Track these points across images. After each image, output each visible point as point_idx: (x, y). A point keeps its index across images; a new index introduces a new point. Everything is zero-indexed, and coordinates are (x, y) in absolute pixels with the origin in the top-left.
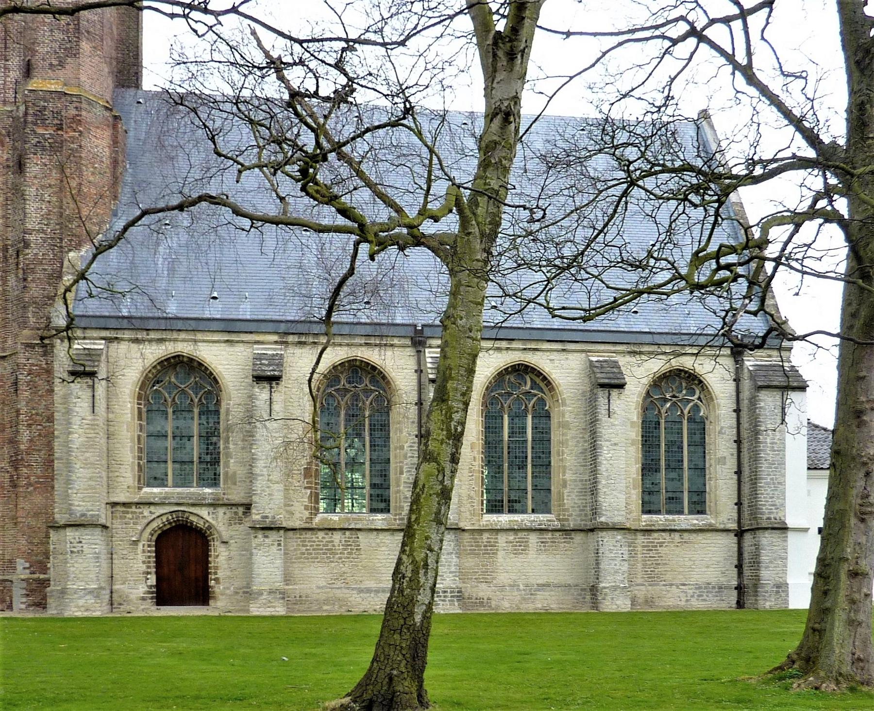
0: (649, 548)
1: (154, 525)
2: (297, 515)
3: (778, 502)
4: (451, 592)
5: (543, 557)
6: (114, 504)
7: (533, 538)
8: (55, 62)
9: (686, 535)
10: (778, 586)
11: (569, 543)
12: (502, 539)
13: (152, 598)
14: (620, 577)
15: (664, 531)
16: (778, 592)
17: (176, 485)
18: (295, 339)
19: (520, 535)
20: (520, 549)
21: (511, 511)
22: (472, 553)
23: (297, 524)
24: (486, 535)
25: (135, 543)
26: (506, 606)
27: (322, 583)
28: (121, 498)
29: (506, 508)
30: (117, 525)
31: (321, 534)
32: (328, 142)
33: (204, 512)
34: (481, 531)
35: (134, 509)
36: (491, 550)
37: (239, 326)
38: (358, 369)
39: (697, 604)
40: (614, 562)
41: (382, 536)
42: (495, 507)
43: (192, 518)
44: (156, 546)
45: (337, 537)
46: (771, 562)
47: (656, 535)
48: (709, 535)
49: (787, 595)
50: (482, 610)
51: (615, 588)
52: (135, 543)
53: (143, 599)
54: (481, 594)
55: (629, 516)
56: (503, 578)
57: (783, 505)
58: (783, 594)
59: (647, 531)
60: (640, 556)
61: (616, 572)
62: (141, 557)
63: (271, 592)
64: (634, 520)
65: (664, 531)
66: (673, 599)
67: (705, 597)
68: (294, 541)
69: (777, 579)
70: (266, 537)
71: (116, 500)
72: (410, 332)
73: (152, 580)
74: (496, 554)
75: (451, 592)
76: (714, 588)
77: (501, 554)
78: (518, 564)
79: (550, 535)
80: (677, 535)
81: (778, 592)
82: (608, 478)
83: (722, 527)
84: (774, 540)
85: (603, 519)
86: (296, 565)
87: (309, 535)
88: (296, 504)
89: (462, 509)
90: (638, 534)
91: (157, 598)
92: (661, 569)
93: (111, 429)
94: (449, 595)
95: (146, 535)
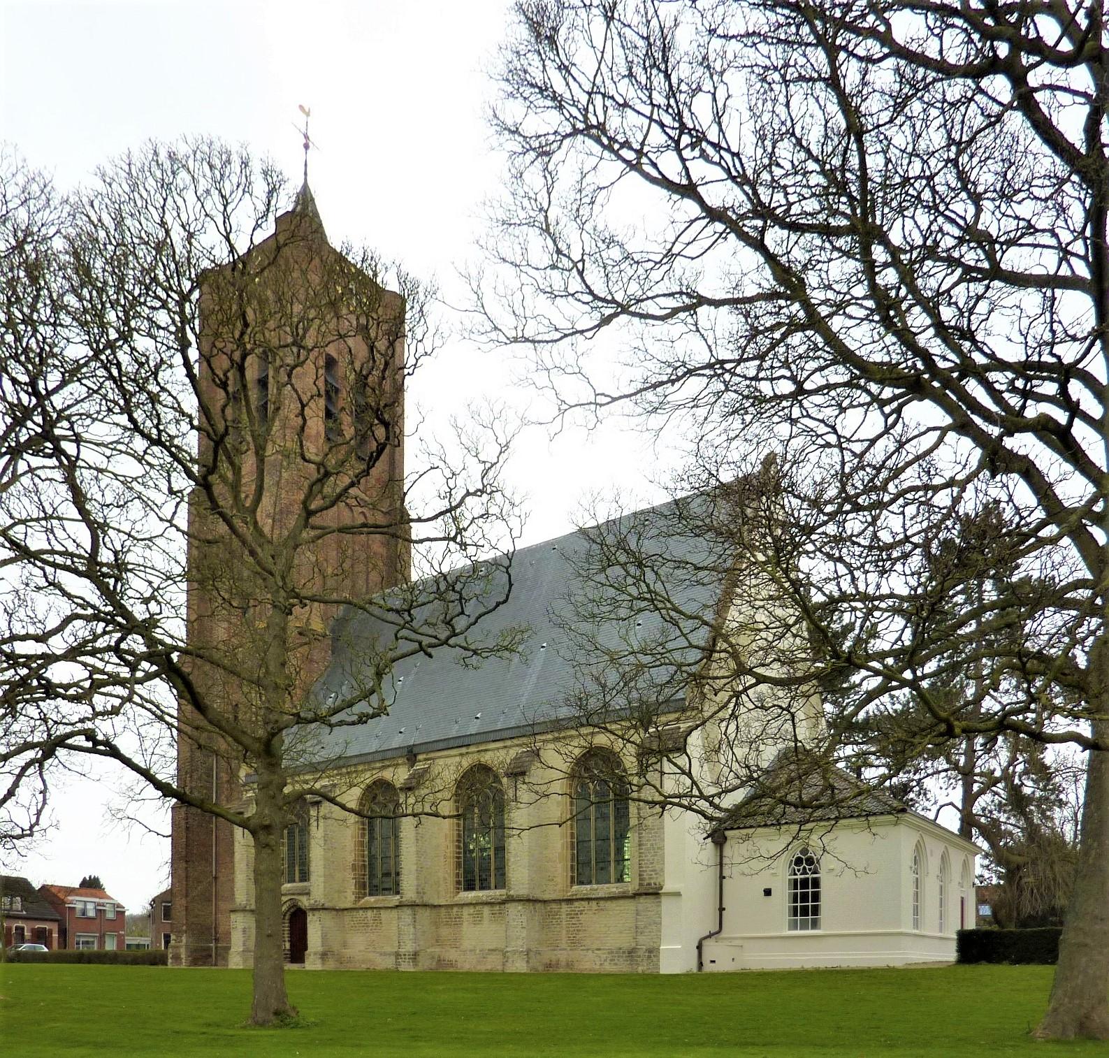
0: (571, 916)
3: (657, 867)
7: (486, 910)
9: (602, 903)
10: (650, 951)
12: (466, 912)
14: (520, 942)
15: (582, 899)
16: (649, 957)
18: (378, 765)
19: (478, 908)
20: (477, 919)
21: (482, 888)
24: (455, 909)
27: (362, 948)
32: (995, 424)
36: (457, 922)
37: (431, 747)
38: (593, 753)
39: (609, 968)
42: (470, 887)
45: (369, 913)
47: (576, 904)
48: (621, 902)
50: (451, 970)
51: (515, 952)
56: (466, 944)
57: (662, 870)
59: (569, 901)
65: (582, 899)
66: (590, 962)
72: (405, 752)
77: (465, 924)
80: (594, 903)
81: (649, 957)
82: (516, 855)
92: (581, 935)
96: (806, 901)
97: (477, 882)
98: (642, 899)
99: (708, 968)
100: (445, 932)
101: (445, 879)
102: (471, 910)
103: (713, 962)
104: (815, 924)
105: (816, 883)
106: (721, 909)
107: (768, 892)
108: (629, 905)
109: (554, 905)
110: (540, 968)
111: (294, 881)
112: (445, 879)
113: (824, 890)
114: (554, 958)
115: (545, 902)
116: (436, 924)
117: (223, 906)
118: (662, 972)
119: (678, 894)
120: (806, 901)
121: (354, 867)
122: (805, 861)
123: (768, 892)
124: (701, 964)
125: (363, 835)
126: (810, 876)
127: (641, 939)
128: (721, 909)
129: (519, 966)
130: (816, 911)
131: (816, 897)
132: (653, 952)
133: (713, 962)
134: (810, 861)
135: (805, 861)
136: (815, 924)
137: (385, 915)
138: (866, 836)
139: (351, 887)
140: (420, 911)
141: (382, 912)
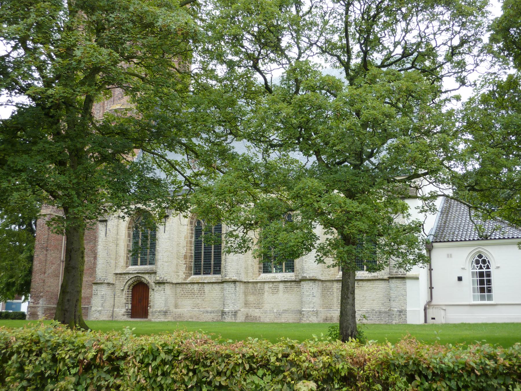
1: (129, 282)
2: (181, 277)
4: (232, 313)
5: (286, 295)
6: (116, 274)
7: (281, 285)
8: (120, 97)
10: (400, 312)
11: (299, 288)
12: (266, 286)
13: (128, 315)
17: (141, 264)
19: (275, 284)
20: (275, 291)
22: (253, 294)
23: (180, 281)
24: (259, 285)
25: (123, 290)
26: (267, 320)
27: (189, 309)
28: (119, 271)
29: (202, 272)
30: (117, 282)
31: (189, 285)
33: (146, 277)
34: (257, 283)
35: (123, 276)
36: (261, 292)
40: (308, 298)
41: (214, 285)
42: (197, 273)
43: (142, 279)
44: (132, 292)
45: (196, 286)
46: (396, 297)
49: (406, 317)
52: (123, 290)
53: (124, 315)
54: (256, 314)
55: (329, 273)
56: (267, 307)
58: (403, 316)
60: (335, 294)
61: (310, 303)
62: (124, 297)
63: (160, 312)
64: (332, 275)
67: (371, 318)
68: (179, 289)
69: (401, 307)
70: (160, 287)
71: (117, 272)
73: (130, 306)
74: (264, 294)
75: (232, 313)
76: (376, 312)
77: (266, 294)
78: (274, 299)
79: (289, 284)
81: (400, 315)
83: (381, 277)
84: (398, 284)
85: (227, 278)
86: (179, 300)
87: (185, 286)
88: (180, 271)
89: (249, 272)
90: (334, 282)
91: (131, 315)
93: (118, 242)
94: (230, 314)
95: (127, 287)
96: (484, 283)
97: (202, 270)
98: (394, 281)
99: (430, 321)
100: (251, 298)
101: (252, 265)
102: (271, 285)
103: (433, 319)
104: (490, 298)
105: (489, 275)
106: (431, 288)
107: (460, 279)
108: (382, 285)
109: (328, 284)
110: (322, 322)
111: (137, 265)
112: (252, 265)
113: (493, 278)
114: (329, 315)
115: (322, 281)
116: (246, 294)
117: (86, 279)
118: (408, 323)
119: (417, 278)
120: (484, 283)
121: (185, 257)
122: (481, 261)
123: (460, 279)
124: (426, 321)
125: (191, 237)
126: (484, 270)
127: (394, 304)
128: (431, 288)
129: (291, 321)
130: (489, 291)
131: (489, 281)
132: (402, 312)
133: (433, 319)
134: (484, 262)
135: (481, 261)
136: (490, 298)
137: (207, 288)
138: (183, 251)
139: (183, 269)
140: (225, 285)
141: (205, 285)
